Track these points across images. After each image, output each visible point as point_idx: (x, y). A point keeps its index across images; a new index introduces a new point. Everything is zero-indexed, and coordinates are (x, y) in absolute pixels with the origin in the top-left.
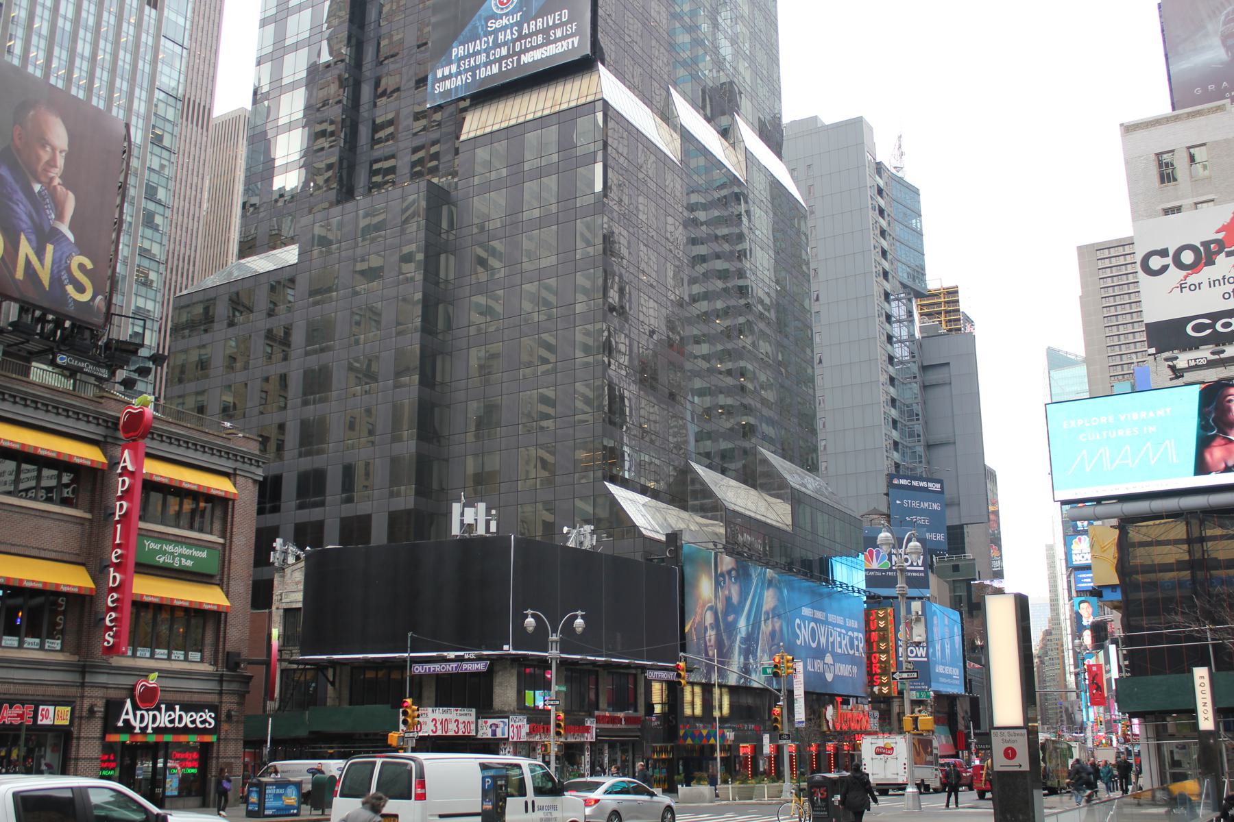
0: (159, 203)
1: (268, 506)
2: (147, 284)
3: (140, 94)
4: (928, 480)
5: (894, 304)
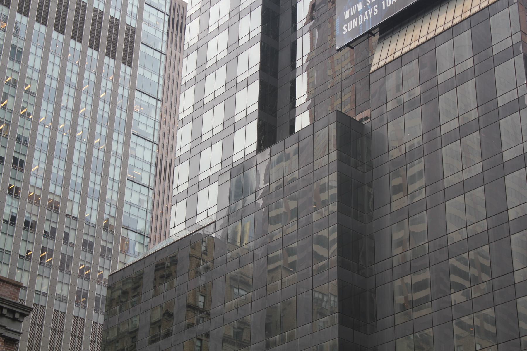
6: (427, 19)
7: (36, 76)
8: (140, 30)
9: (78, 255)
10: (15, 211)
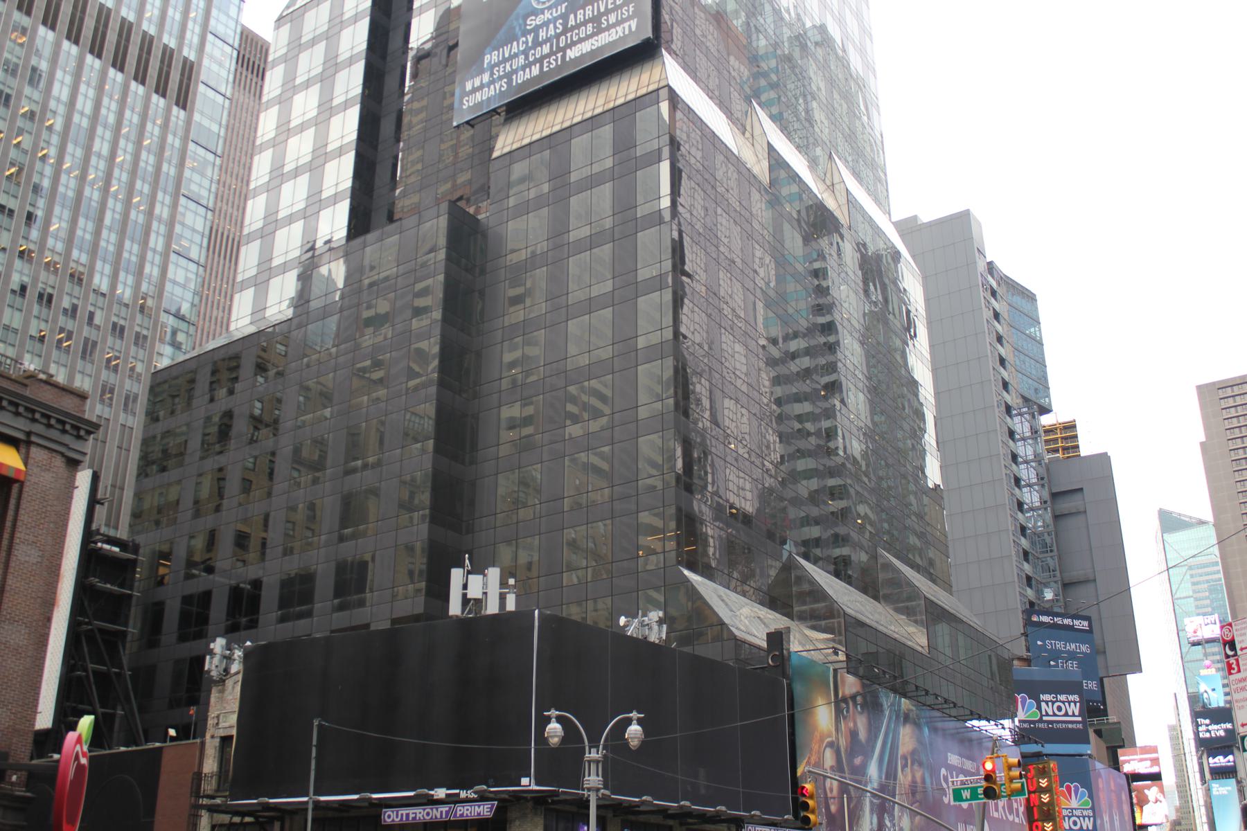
1: (244, 620)
4: (1074, 617)
5: (1017, 419)
6: (564, 103)
7: (61, 110)
8: (200, 65)
9: (104, 340)
10: (25, 279)
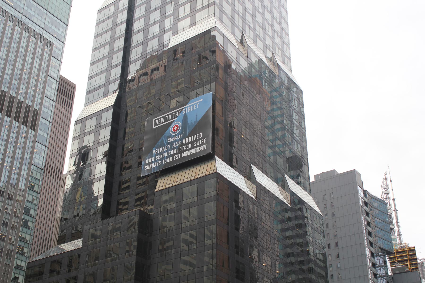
0: (31, 216)
2: (23, 254)
3: (25, 168)
